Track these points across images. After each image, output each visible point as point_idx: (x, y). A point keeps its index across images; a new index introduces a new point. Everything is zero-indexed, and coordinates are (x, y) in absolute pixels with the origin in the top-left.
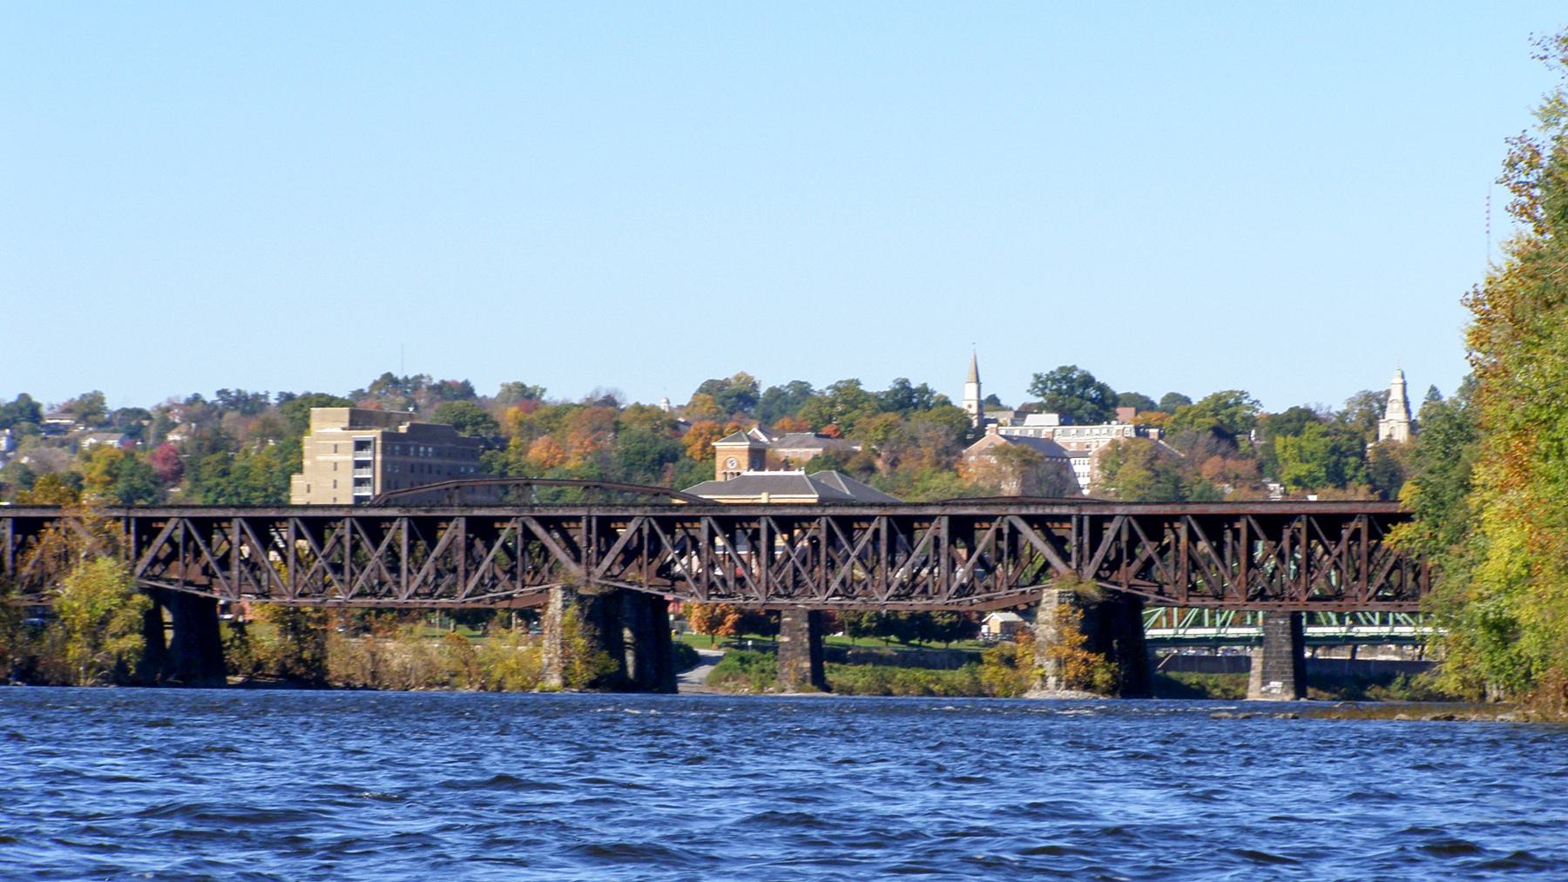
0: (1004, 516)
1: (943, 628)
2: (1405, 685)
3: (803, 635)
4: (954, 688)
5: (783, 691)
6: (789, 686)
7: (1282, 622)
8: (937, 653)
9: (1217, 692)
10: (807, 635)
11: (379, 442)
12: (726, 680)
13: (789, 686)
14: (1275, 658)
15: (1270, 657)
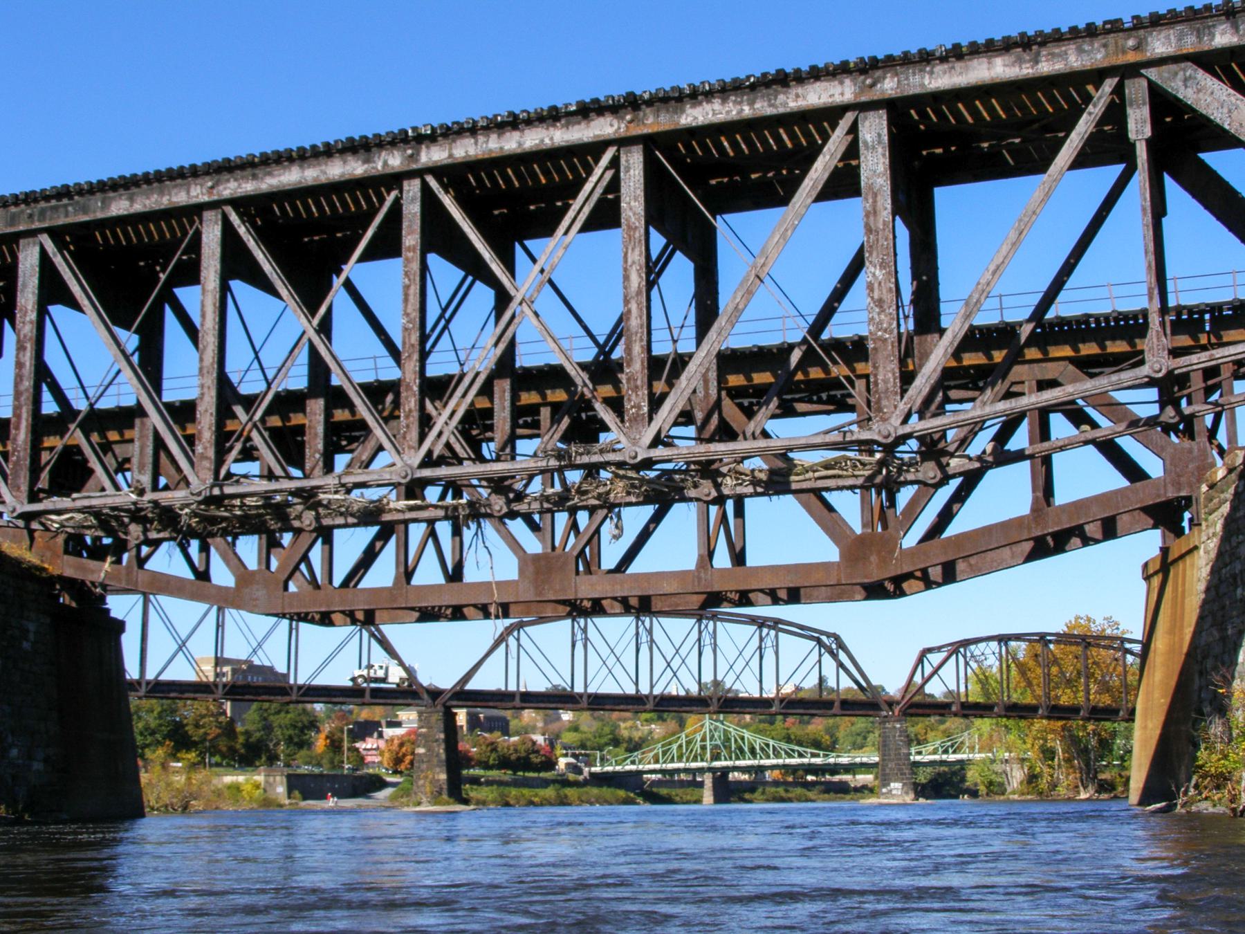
0: (1132, 71)
1: (537, 764)
2: (763, 793)
3: (439, 746)
4: (546, 799)
5: (419, 804)
6: (424, 799)
7: (898, 726)
8: (533, 779)
9: (678, 799)
10: (443, 746)
11: (230, 673)
12: (402, 797)
13: (424, 799)
14: (893, 760)
15: (890, 760)
